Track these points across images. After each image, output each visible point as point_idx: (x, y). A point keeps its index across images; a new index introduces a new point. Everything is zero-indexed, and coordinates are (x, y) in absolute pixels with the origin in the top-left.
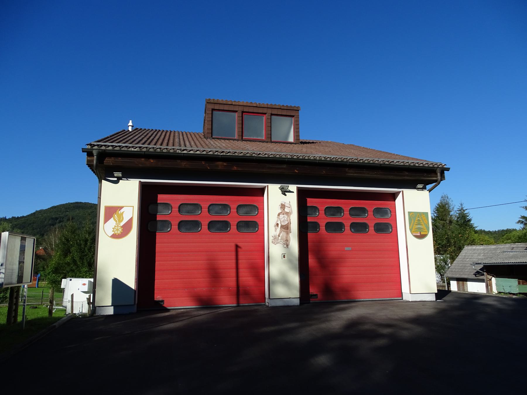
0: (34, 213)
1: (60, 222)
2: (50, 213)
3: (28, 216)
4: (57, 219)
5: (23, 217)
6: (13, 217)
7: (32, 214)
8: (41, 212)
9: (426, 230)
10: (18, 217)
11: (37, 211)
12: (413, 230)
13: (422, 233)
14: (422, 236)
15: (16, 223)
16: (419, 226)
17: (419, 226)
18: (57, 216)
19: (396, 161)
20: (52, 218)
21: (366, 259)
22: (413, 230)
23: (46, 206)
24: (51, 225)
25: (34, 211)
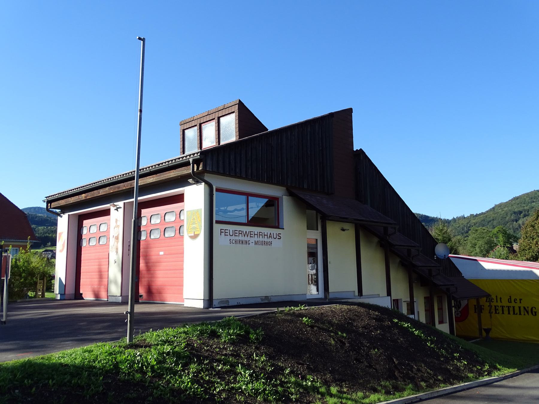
0: (493, 208)
1: (525, 216)
2: (512, 205)
3: (487, 212)
4: (521, 212)
5: (482, 213)
6: (471, 215)
7: (491, 210)
8: (500, 206)
9: (198, 230)
10: (477, 215)
11: (496, 206)
12: (189, 230)
13: (196, 233)
14: (271, 243)
15: (474, 221)
16: (194, 225)
17: (194, 225)
18: (521, 209)
19: (85, 314)
20: (515, 213)
21: (173, 247)
22: (189, 230)
23: (505, 199)
24: (513, 221)
25: (493, 206)
